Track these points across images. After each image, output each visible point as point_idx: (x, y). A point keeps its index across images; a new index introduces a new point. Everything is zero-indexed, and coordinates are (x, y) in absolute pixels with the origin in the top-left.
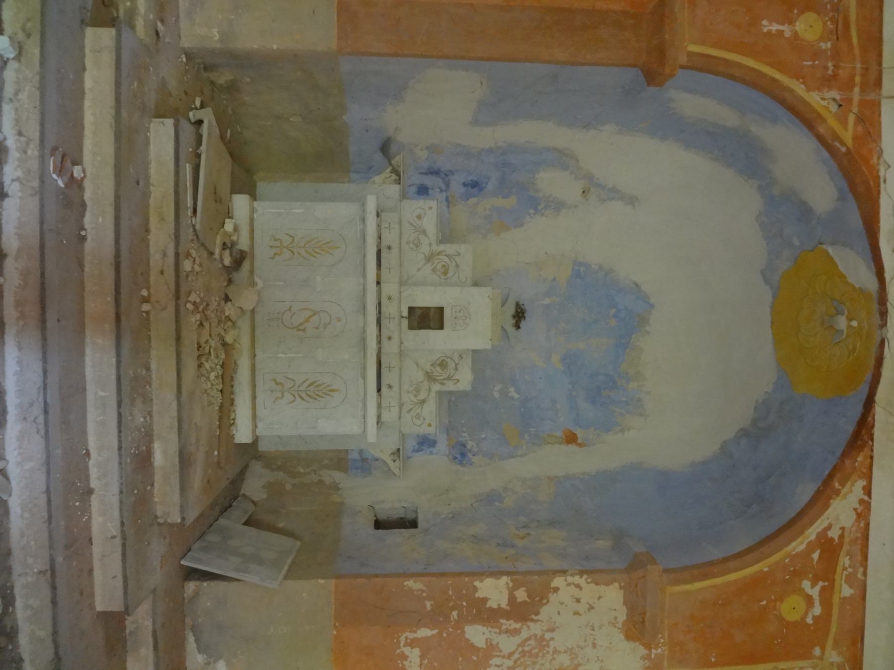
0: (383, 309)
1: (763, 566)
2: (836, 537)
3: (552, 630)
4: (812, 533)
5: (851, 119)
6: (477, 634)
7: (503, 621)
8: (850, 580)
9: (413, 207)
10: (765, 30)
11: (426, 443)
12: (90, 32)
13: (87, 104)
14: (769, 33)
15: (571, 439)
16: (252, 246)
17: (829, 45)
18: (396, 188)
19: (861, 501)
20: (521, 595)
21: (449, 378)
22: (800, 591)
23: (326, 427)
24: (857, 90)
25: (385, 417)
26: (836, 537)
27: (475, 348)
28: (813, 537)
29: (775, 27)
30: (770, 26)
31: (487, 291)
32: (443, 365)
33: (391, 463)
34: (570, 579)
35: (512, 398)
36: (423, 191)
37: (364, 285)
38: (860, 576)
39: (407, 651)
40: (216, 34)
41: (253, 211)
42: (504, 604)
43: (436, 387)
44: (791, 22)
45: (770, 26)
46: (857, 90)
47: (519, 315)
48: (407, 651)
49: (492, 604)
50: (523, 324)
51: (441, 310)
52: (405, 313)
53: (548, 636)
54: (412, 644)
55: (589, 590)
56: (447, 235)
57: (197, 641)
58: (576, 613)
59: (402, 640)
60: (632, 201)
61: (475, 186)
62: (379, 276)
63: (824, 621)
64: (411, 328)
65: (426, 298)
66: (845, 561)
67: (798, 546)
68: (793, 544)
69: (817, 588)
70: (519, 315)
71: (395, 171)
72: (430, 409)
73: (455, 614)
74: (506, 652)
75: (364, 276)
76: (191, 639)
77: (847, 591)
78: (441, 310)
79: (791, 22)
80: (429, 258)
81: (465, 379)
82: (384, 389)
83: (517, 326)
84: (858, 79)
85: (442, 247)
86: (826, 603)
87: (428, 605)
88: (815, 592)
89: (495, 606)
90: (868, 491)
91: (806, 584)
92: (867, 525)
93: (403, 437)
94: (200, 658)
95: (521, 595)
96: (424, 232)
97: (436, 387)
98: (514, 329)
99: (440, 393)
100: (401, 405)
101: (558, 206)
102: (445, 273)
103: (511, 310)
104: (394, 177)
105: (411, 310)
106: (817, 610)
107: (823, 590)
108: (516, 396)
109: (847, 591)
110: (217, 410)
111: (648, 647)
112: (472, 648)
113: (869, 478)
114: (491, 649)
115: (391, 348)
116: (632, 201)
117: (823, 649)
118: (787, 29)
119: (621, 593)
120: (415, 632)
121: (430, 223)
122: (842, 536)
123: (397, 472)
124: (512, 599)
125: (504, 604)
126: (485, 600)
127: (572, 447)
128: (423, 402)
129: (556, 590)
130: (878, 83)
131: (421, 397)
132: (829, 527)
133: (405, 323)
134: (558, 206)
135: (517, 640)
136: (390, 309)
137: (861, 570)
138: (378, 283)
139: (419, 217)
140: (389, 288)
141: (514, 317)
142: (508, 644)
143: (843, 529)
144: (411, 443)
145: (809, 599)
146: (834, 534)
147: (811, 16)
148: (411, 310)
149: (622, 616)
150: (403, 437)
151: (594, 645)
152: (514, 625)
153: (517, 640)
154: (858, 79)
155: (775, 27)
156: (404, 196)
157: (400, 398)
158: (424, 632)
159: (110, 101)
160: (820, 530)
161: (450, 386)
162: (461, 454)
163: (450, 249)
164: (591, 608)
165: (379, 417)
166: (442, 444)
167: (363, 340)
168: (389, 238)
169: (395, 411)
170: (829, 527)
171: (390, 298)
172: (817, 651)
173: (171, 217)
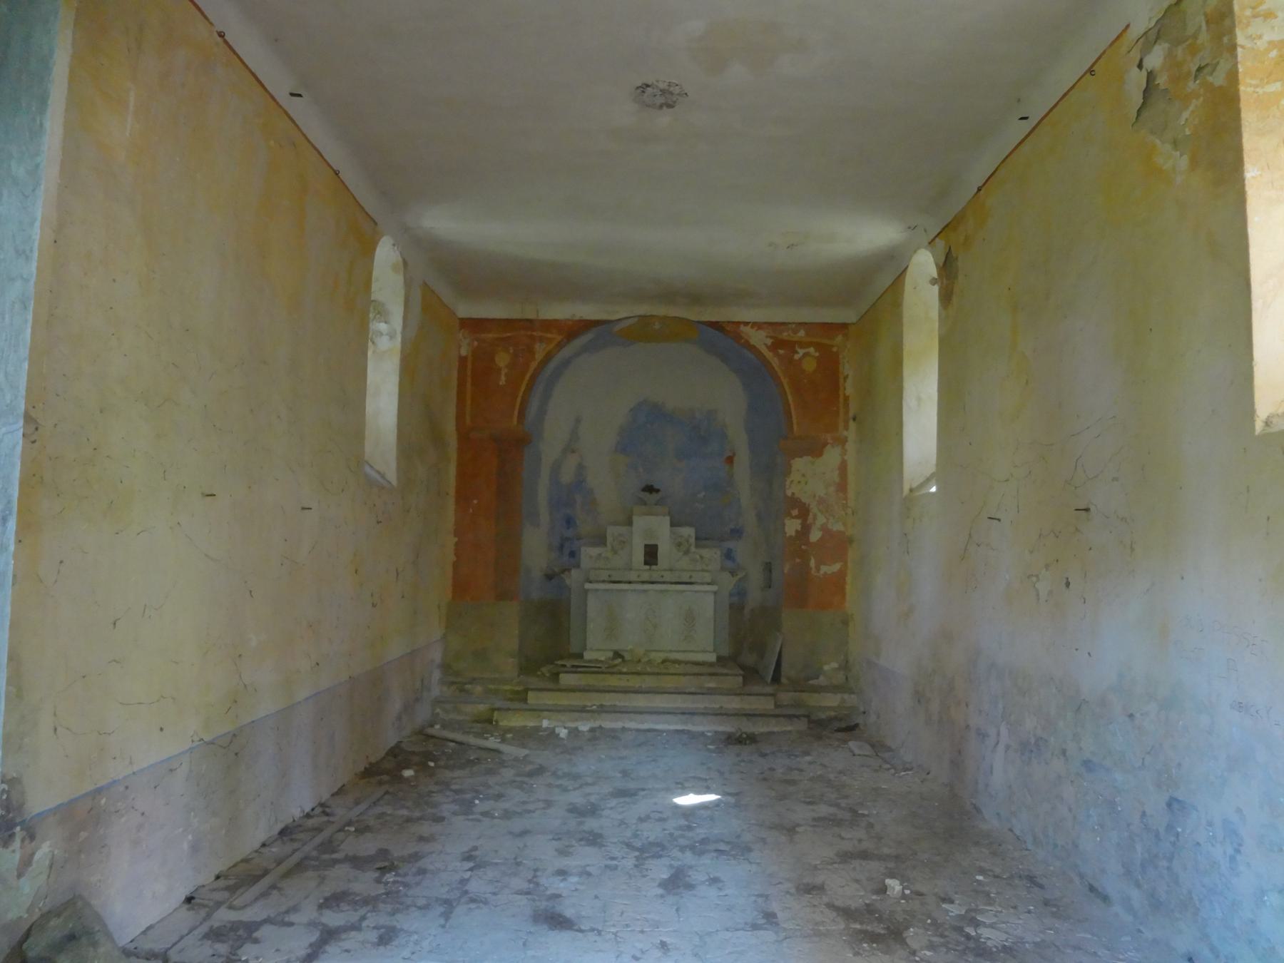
0: (645, 580)
1: (785, 381)
2: (771, 341)
3: (815, 496)
4: (768, 355)
5: (549, 335)
6: (815, 536)
7: (808, 522)
8: (795, 332)
9: (585, 562)
10: (504, 383)
11: (729, 555)
12: (529, 702)
13: (559, 703)
14: (506, 381)
15: (730, 460)
16: (612, 650)
17: (511, 348)
18: (573, 572)
19: (752, 327)
20: (795, 512)
21: (688, 541)
22: (800, 359)
23: (710, 612)
24: (535, 333)
25: (709, 580)
26: (771, 341)
27: (669, 526)
28: (771, 354)
29: (503, 378)
30: (503, 380)
31: (635, 518)
32: (679, 545)
33: (739, 577)
34: (787, 487)
35: (704, 496)
36: (573, 554)
37: (632, 591)
38: (794, 326)
39: (822, 572)
40: (511, 660)
41: (591, 649)
42: (799, 521)
43: (693, 549)
44: (500, 370)
45: (503, 380)
46: (535, 333)
47: (650, 489)
48: (822, 572)
49: (799, 528)
50: (656, 487)
51: (646, 546)
52: (648, 567)
53: (817, 498)
54: (818, 569)
55: (794, 476)
56: (600, 540)
57: (812, 679)
58: (806, 483)
59: (816, 574)
60: (578, 420)
61: (569, 522)
62: (626, 582)
63: (818, 346)
64: (656, 564)
65: (639, 556)
66: (785, 335)
67: (775, 362)
68: (774, 365)
69: (799, 350)
70: (650, 489)
71: (563, 571)
72: (706, 553)
73: (803, 547)
74: (825, 521)
75: (627, 590)
76: (811, 682)
77: (802, 333)
78: (646, 546)
79: (500, 370)
80: (615, 552)
81: (688, 532)
82: (693, 580)
83: (658, 491)
84: (529, 333)
85: (608, 544)
86: (809, 344)
87: (798, 560)
88: (801, 352)
89: (800, 526)
90: (746, 324)
91: (797, 357)
92: (765, 323)
93: (723, 569)
94: (822, 678)
95: (795, 512)
96: (600, 555)
97: (693, 549)
98: (660, 493)
99: (697, 546)
100: (703, 570)
101: (581, 467)
102: (624, 542)
103: (646, 496)
104: (567, 573)
105: (646, 563)
106: (812, 350)
107: (801, 348)
108: (703, 493)
109: (802, 333)
110: (878, 946)
111: (825, 444)
112: (821, 539)
113: (739, 323)
114: (824, 529)
115: (668, 576)
116: (578, 420)
117: (833, 346)
118: (504, 372)
119: (797, 459)
120: (811, 569)
121: (594, 551)
122: (771, 337)
123: (744, 574)
124: (796, 517)
125: (799, 521)
126: (797, 531)
127: (736, 459)
128: (702, 557)
129: (793, 494)
130: (530, 321)
131: (698, 557)
132: (765, 344)
133: (654, 567)
134: (581, 467)
135: (819, 514)
136: (645, 576)
137: (790, 325)
138: (630, 582)
139: (591, 557)
140: (633, 576)
141: (651, 493)
142: (821, 520)
143: (767, 337)
144: (729, 564)
145: (805, 355)
146: (769, 342)
147: (497, 359)
148: (646, 563)
149: (809, 458)
150: (723, 569)
151: (824, 473)
152: (811, 516)
153: (819, 514)
154: (529, 333)
155: (503, 378)
156: (578, 566)
157: (698, 571)
158: (812, 563)
159: (559, 694)
160: (767, 350)
161: (692, 540)
162: (737, 533)
163: (609, 539)
164: (804, 475)
165: (709, 584)
166: (729, 544)
167: (662, 591)
168: (604, 575)
169: (706, 574)
170: (765, 344)
171: (639, 576)
172: (835, 349)
173: (604, 676)
